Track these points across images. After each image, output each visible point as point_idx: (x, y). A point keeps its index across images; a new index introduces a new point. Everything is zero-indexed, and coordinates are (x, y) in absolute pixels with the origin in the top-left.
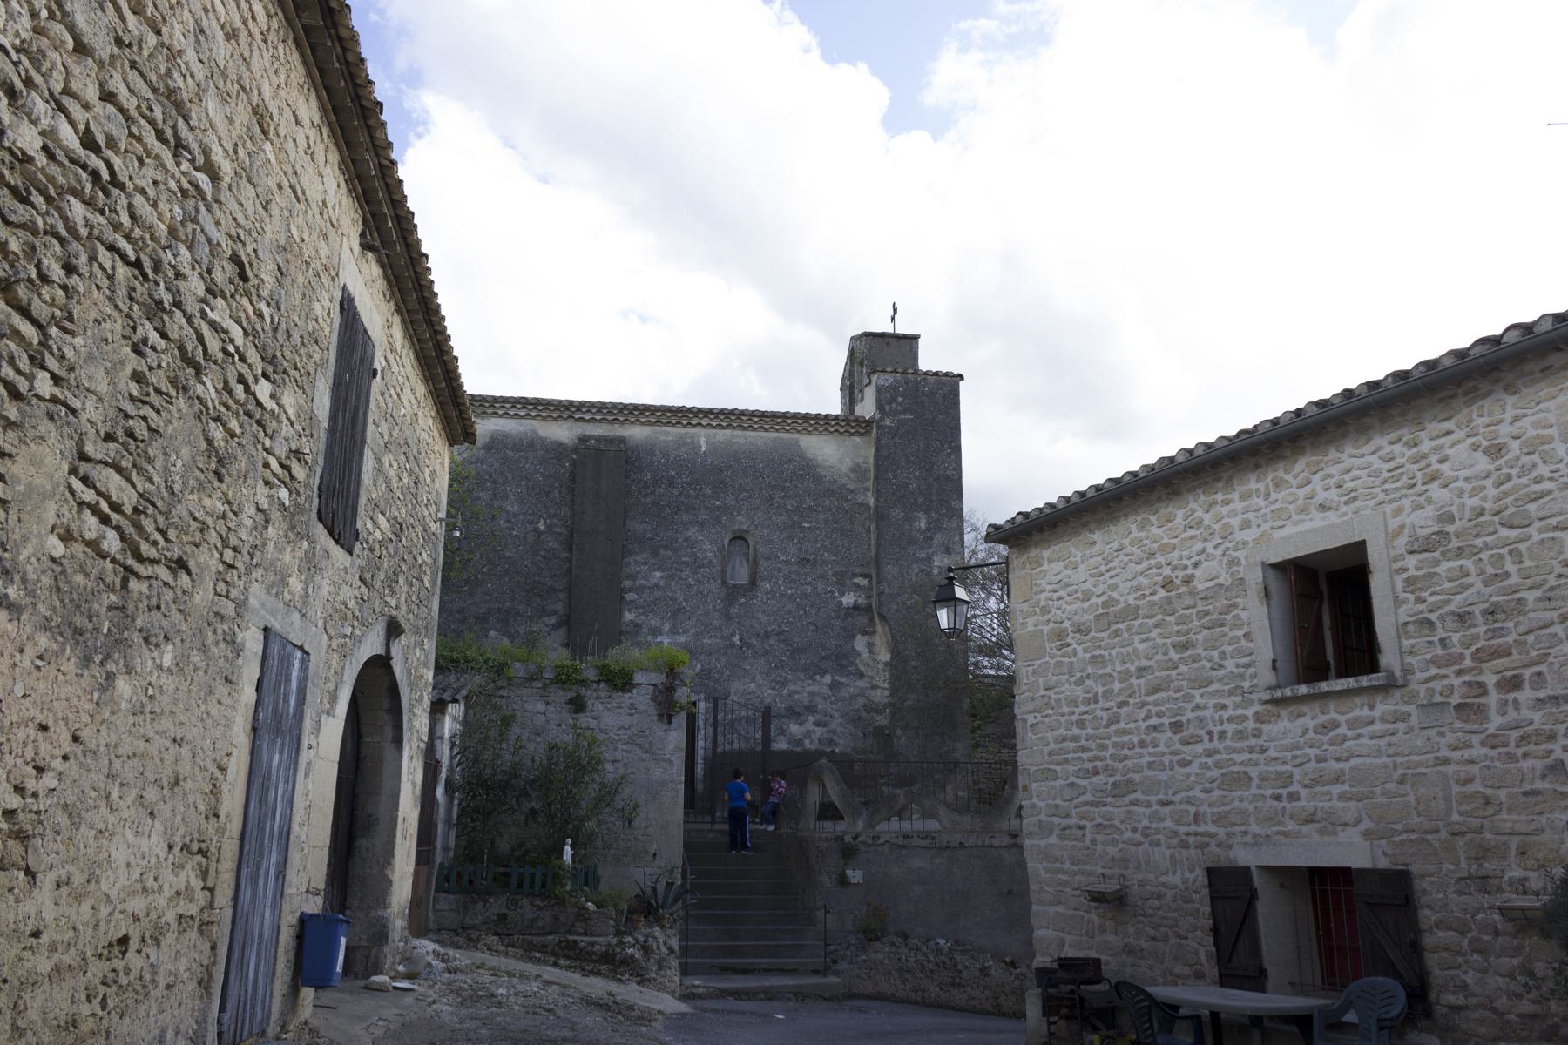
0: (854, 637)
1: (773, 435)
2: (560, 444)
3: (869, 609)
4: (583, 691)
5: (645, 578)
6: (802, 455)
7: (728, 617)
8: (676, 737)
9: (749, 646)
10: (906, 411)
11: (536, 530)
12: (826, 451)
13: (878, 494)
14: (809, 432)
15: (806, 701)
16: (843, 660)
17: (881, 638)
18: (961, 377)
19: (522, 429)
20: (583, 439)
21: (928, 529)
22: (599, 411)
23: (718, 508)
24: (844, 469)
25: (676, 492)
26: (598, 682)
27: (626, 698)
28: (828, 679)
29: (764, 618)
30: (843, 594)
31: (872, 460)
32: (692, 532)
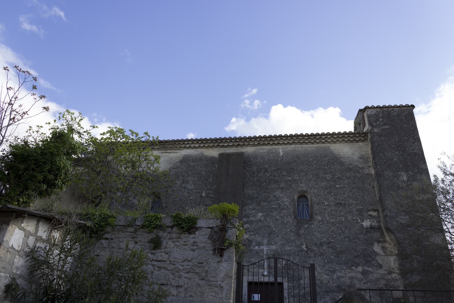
0: (372, 244)
1: (316, 145)
2: (214, 158)
3: (379, 228)
4: (161, 233)
5: (254, 216)
6: (332, 153)
7: (298, 235)
8: (228, 266)
9: (312, 251)
10: (385, 124)
11: (201, 196)
12: (344, 150)
13: (375, 165)
14: (335, 142)
15: (348, 282)
16: (368, 258)
17: (391, 246)
18: (413, 106)
19: (197, 153)
20: (221, 155)
21: (408, 180)
22: (231, 141)
23: (290, 181)
24: (356, 157)
25: (268, 175)
26: (172, 227)
27: (191, 238)
28: (360, 269)
29: (319, 235)
30: (363, 221)
31: (370, 152)
32: (278, 193)
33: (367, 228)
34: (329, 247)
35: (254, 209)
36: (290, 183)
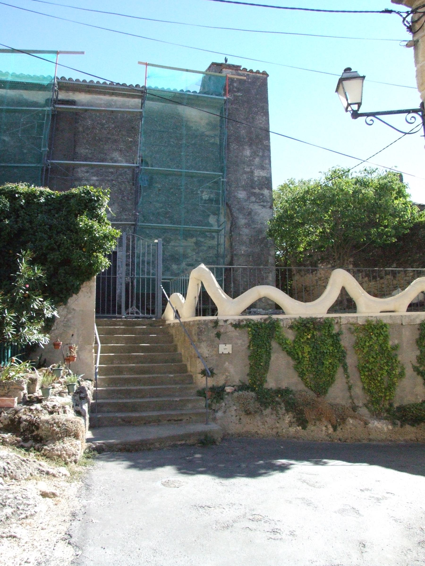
12: (192, 114)
28: (194, 240)
33: (205, 200)
34: (166, 218)
35: (87, 172)
36: (130, 145)
